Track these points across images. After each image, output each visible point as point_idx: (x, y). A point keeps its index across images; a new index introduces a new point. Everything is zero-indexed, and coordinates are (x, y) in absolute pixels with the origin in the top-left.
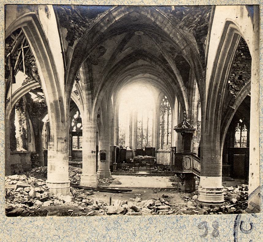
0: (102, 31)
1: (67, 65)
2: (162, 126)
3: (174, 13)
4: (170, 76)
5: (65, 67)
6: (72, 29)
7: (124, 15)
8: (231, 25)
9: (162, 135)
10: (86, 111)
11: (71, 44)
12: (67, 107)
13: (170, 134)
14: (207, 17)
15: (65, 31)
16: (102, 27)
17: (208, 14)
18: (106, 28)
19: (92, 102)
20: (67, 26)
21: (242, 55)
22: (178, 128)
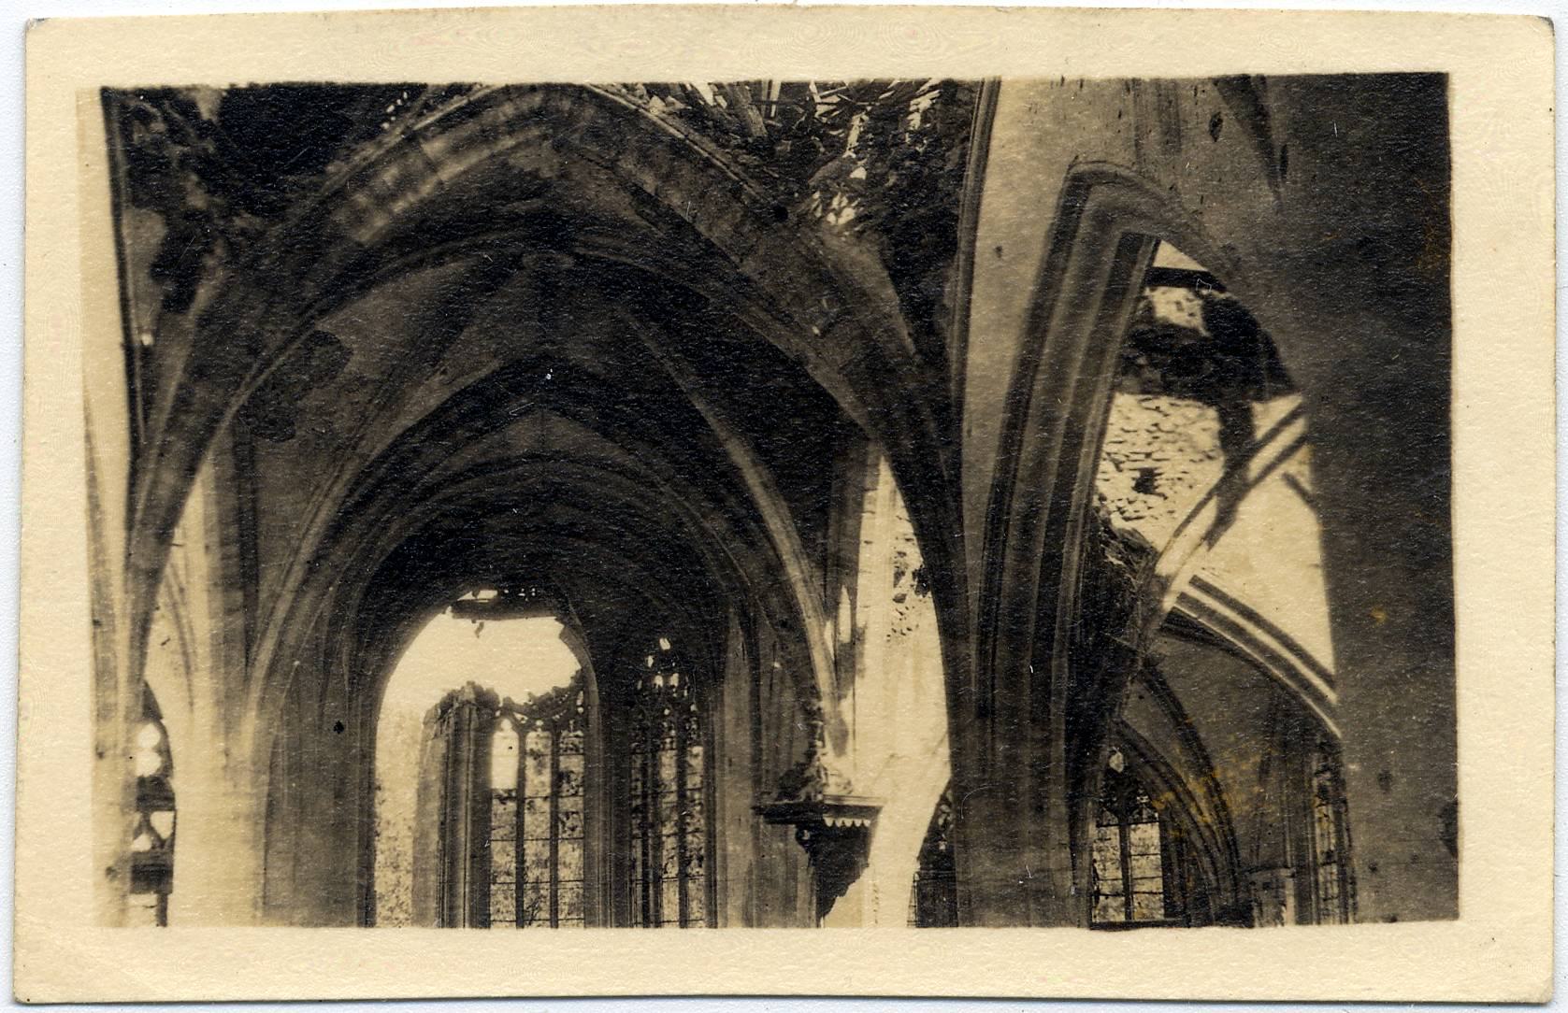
0: (364, 236)
1: (146, 418)
2: (645, 818)
3: (763, 148)
4: (719, 501)
5: (134, 430)
6: (191, 215)
7: (486, 153)
8: (1099, 197)
9: (645, 875)
10: (206, 712)
11: (177, 302)
12: (131, 657)
13: (695, 862)
14: (948, 167)
15: (151, 231)
16: (359, 218)
17: (954, 155)
18: (380, 222)
19: (249, 661)
20: (164, 203)
21: (1141, 366)
22: (779, 798)
